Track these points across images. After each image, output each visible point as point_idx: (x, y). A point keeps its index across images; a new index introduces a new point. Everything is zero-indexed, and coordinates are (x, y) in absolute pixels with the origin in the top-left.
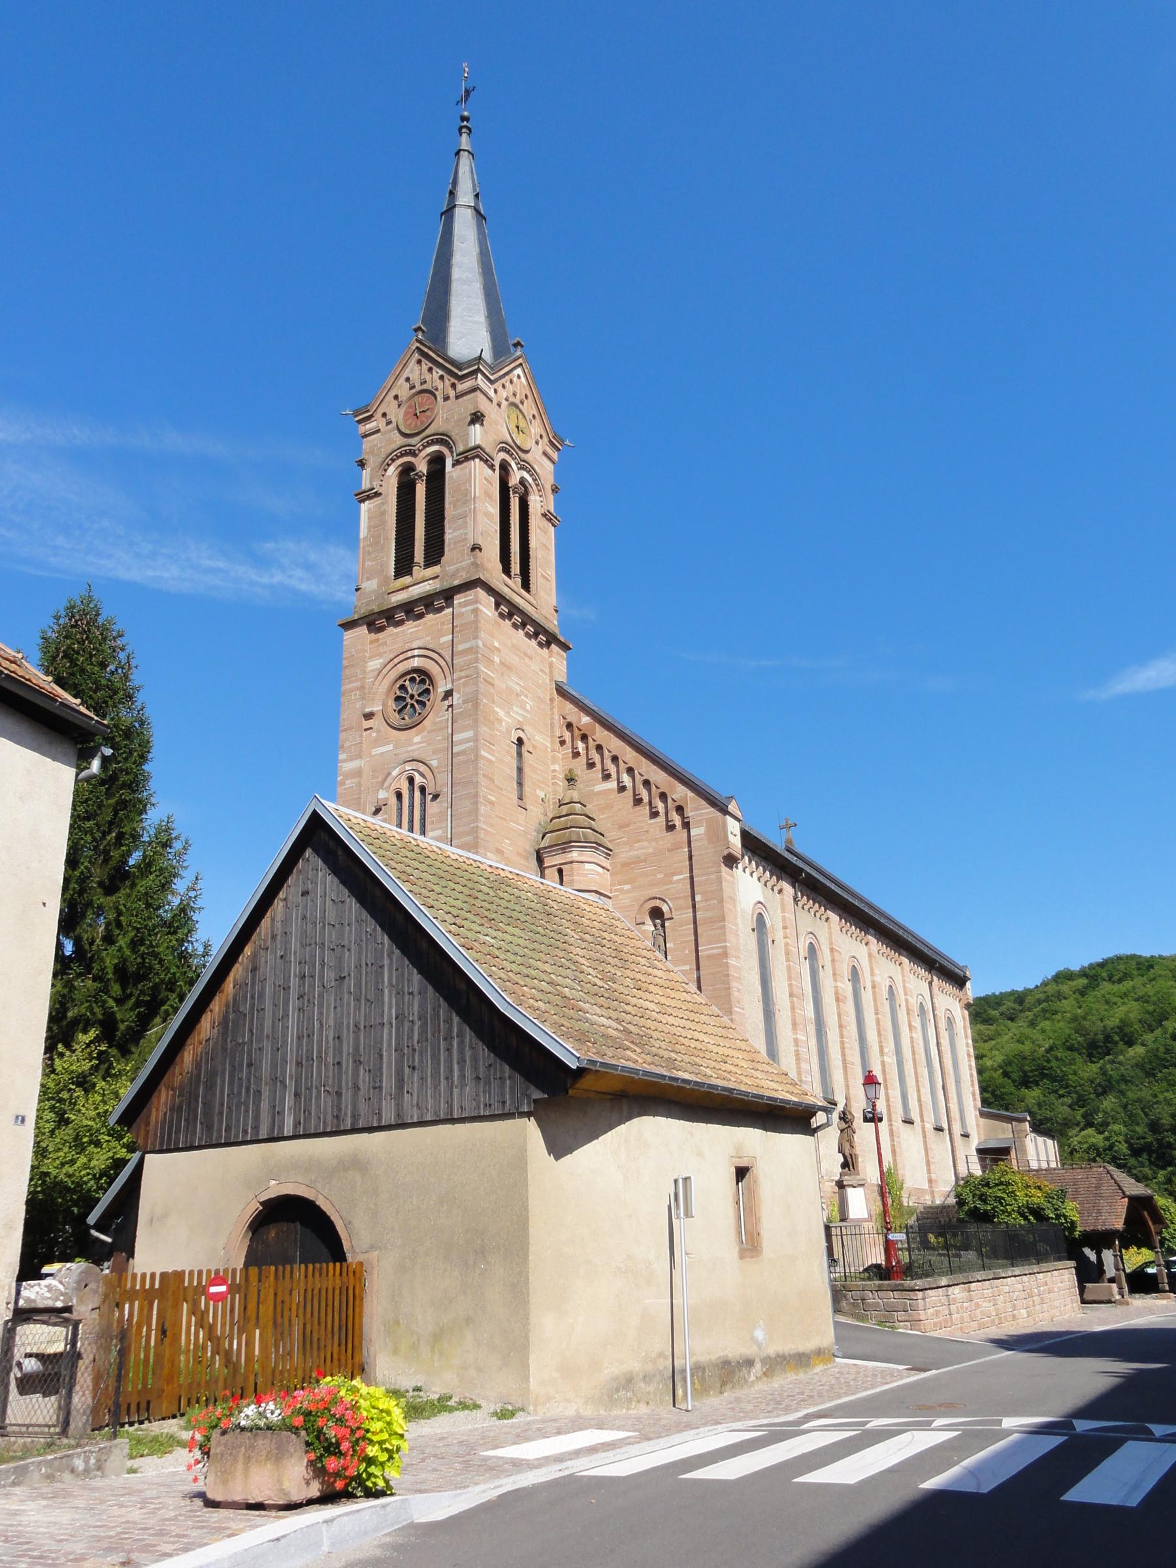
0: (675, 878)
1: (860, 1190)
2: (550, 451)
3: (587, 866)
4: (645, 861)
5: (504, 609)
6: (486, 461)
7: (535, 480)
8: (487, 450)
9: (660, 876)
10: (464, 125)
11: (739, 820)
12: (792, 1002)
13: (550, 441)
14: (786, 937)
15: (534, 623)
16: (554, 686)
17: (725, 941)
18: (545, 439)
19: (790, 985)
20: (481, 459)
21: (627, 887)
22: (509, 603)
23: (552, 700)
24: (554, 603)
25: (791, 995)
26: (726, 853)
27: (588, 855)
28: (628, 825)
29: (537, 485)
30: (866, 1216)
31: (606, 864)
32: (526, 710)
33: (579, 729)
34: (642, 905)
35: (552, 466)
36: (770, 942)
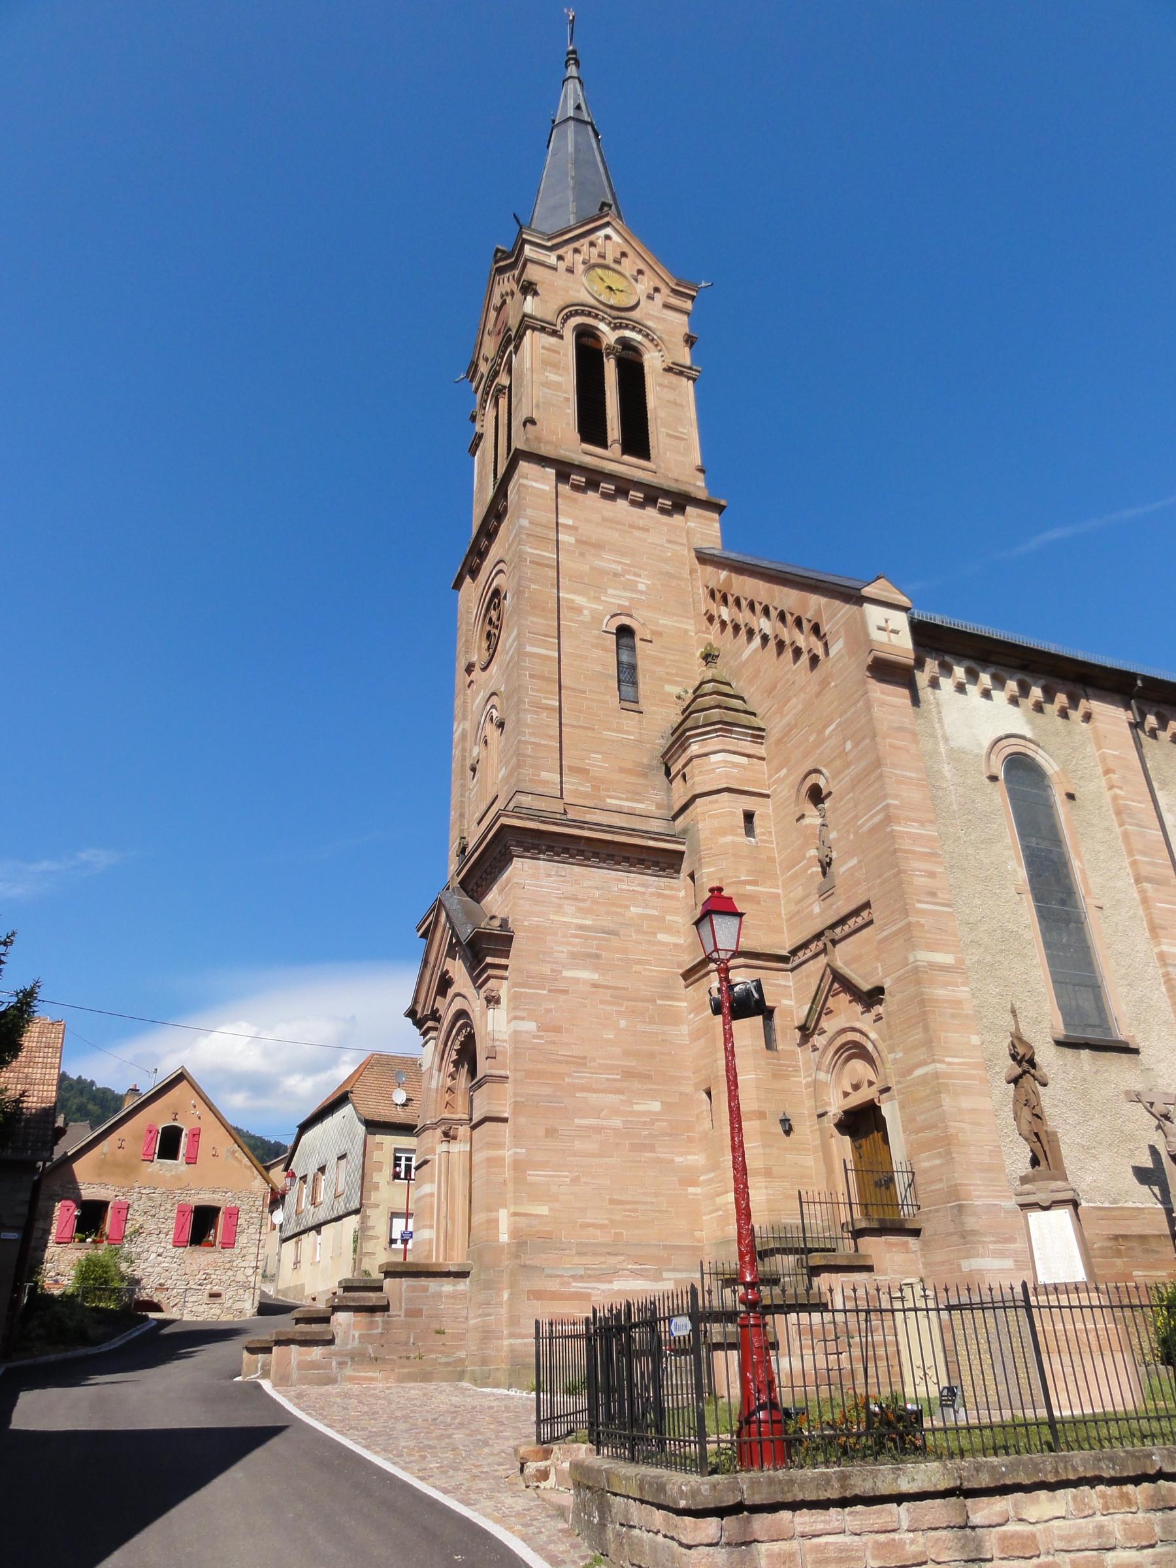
0: (828, 732)
1: (1063, 1216)
2: (675, 301)
3: (713, 758)
4: (795, 726)
5: (639, 495)
6: (543, 330)
7: (647, 336)
8: (539, 316)
9: (812, 738)
10: (574, 58)
11: (905, 609)
12: (1142, 892)
13: (673, 291)
14: (1111, 787)
15: (667, 493)
16: (693, 554)
17: (885, 796)
18: (665, 290)
19: (1134, 863)
20: (534, 329)
21: (784, 771)
22: (581, 469)
23: (692, 571)
24: (698, 462)
25: (1138, 880)
26: (869, 660)
27: (715, 743)
28: (775, 687)
29: (652, 340)
30: (1080, 1276)
31: (760, 750)
32: (641, 592)
33: (776, 609)
34: (799, 791)
35: (685, 318)
36: (1058, 798)
